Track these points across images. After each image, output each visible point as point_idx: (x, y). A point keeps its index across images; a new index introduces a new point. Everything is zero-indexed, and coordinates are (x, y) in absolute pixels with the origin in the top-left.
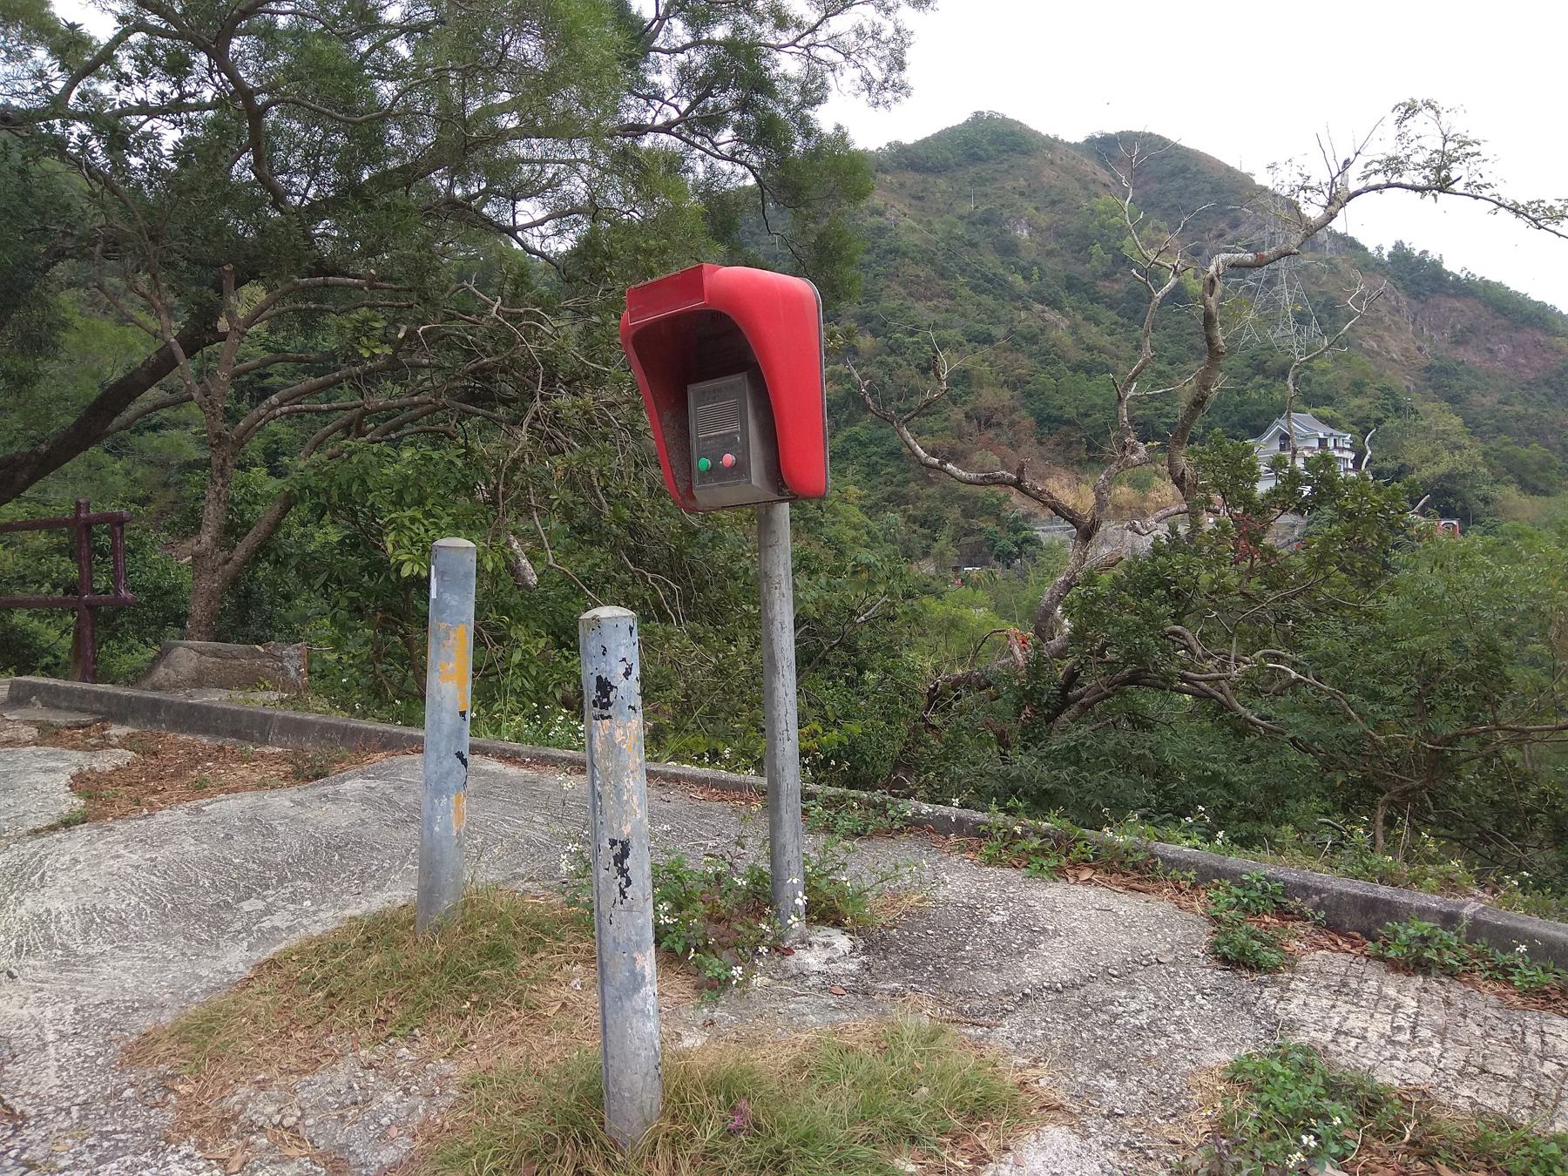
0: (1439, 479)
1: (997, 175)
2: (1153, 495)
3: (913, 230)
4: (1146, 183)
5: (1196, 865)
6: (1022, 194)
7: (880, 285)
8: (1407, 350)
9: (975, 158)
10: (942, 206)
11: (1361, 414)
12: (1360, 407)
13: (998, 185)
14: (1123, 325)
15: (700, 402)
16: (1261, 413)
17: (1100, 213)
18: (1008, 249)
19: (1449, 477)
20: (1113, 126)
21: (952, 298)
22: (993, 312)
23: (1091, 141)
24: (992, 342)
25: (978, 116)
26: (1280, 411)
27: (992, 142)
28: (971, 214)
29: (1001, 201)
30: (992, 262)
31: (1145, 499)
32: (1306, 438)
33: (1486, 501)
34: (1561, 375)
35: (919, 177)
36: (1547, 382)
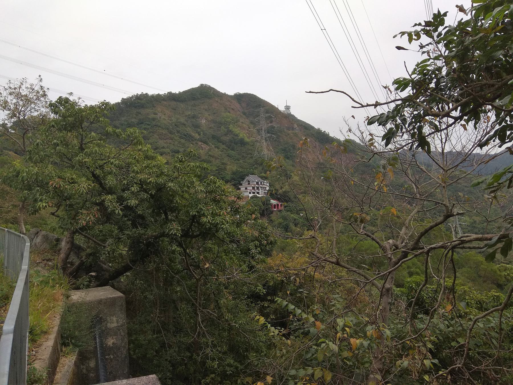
5: (488, 84)
9: (194, 99)
10: (181, 112)
13: (199, 107)
18: (197, 126)
21: (172, 139)
23: (236, 95)
25: (202, 85)
30: (190, 130)
35: (175, 103)
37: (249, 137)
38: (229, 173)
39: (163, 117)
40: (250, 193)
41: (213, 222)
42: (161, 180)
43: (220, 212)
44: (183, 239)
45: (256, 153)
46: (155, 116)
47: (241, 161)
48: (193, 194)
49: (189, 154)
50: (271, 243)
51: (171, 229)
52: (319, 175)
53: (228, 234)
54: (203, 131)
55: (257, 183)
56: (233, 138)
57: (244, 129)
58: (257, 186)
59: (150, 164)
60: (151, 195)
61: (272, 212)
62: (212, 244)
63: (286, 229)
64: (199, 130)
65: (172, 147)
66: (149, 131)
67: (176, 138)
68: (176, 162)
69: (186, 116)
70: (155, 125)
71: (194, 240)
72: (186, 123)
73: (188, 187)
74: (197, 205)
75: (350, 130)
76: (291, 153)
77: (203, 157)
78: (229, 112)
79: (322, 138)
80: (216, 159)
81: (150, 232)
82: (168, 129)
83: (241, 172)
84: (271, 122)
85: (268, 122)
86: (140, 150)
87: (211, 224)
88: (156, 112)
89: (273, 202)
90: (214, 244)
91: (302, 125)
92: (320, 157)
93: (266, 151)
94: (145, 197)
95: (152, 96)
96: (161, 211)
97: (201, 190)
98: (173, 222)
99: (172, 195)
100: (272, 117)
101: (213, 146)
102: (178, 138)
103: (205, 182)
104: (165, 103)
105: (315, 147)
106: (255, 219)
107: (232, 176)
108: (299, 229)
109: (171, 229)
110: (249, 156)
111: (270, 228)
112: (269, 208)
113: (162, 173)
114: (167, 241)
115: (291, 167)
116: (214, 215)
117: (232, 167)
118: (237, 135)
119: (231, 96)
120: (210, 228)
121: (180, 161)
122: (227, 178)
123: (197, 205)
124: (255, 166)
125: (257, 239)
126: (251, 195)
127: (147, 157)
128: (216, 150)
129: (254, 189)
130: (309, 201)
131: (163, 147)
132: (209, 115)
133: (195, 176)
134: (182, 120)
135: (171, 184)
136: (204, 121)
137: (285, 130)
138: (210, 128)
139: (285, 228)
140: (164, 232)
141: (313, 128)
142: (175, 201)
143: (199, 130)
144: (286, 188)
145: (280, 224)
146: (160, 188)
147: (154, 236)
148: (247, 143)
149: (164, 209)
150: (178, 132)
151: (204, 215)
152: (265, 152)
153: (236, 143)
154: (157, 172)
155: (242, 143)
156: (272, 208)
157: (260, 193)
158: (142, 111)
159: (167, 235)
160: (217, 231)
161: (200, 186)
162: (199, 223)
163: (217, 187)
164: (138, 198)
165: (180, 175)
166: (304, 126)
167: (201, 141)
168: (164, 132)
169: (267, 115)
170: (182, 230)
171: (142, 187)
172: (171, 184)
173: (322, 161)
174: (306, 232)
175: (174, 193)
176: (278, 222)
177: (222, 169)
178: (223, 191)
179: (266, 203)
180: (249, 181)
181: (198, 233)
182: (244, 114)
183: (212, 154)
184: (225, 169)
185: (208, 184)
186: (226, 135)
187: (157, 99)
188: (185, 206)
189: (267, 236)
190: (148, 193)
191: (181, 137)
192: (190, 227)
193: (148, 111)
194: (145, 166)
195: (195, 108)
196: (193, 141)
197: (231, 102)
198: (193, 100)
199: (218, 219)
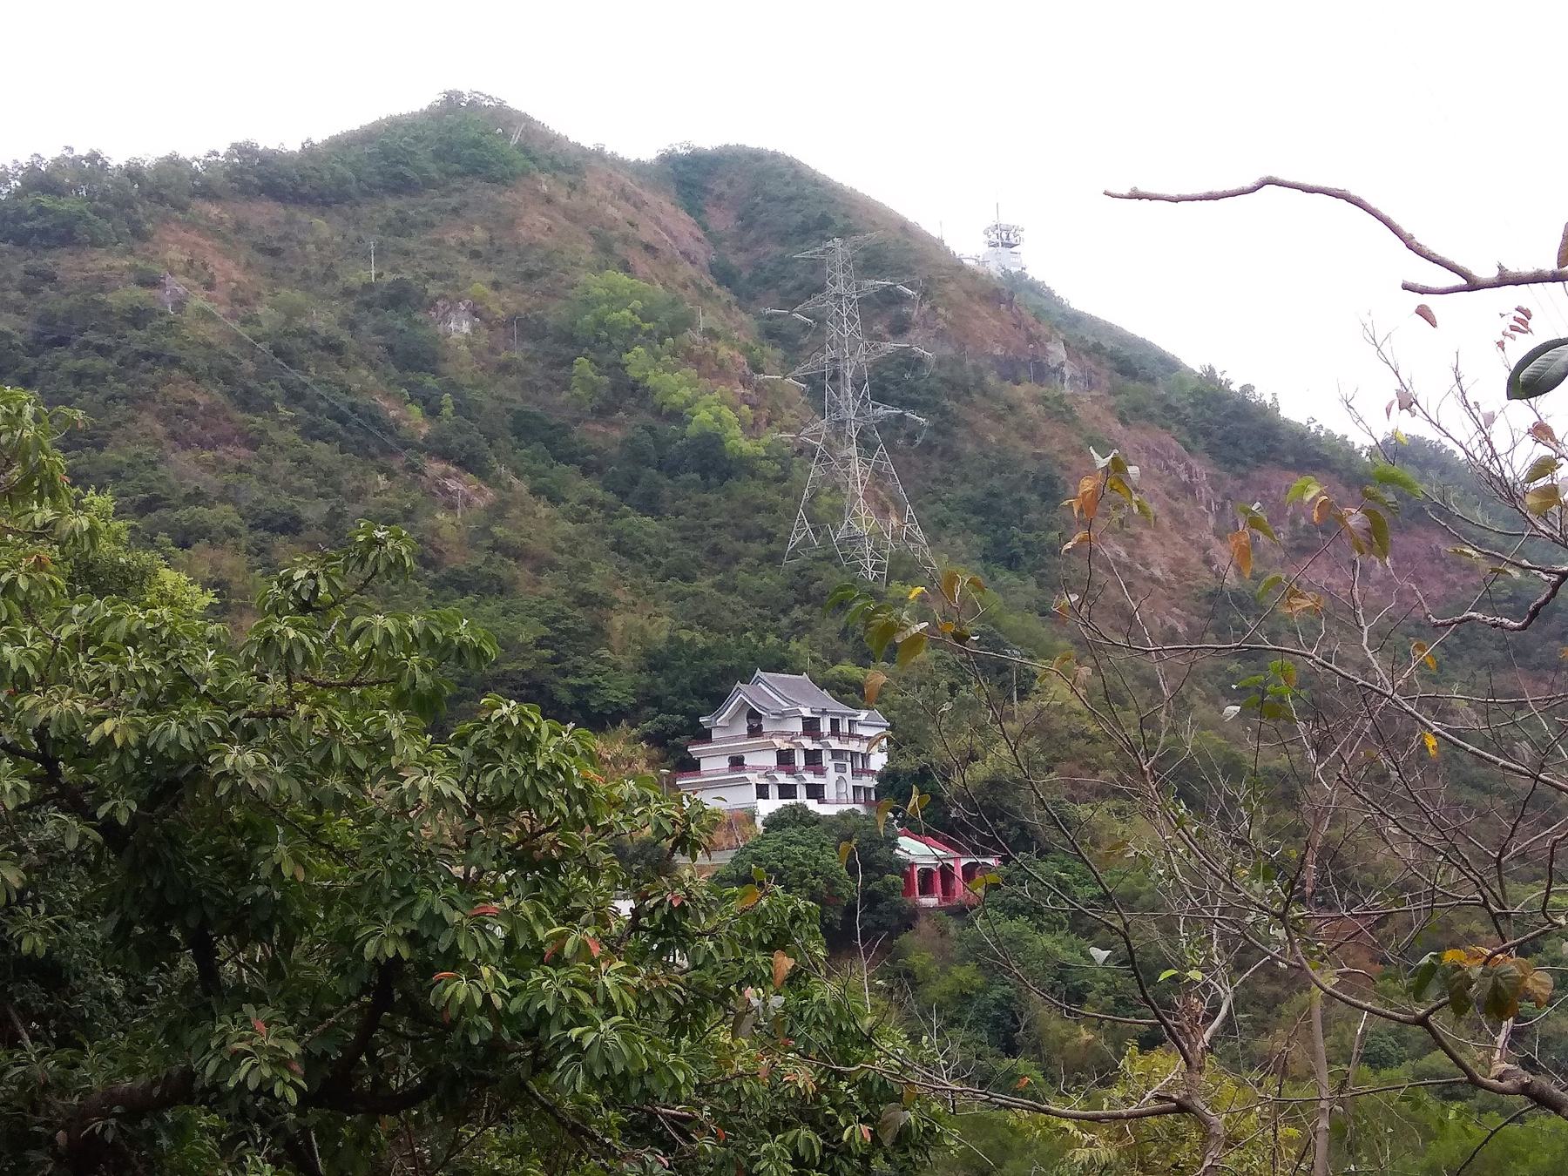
1: (435, 218)
3: (206, 316)
4: (758, 241)
6: (475, 255)
7: (115, 418)
8: (1181, 562)
9: (401, 185)
13: (434, 235)
14: (602, 506)
17: (598, 301)
18: (414, 360)
20: (708, 139)
21: (253, 445)
22: (329, 473)
23: (670, 162)
24: (296, 532)
25: (452, 100)
27: (438, 156)
28: (368, 287)
29: (430, 266)
30: (369, 386)
35: (279, 211)
37: (751, 429)
38: (626, 661)
39: (198, 300)
40: (762, 792)
41: (516, 1005)
42: (173, 730)
43: (563, 937)
44: (314, 1115)
45: (799, 532)
46: (143, 293)
47: (704, 584)
48: (387, 819)
49: (363, 560)
50: (903, 1137)
51: (239, 1056)
52: (1218, 670)
53: (616, 1086)
54: (453, 387)
55: (811, 727)
56: (651, 429)
57: (720, 372)
58: (808, 744)
59: (105, 623)
60: (109, 827)
61: (909, 919)
62: (509, 1151)
63: (1007, 1031)
64: (430, 382)
65: (255, 491)
66: (104, 392)
67: (277, 436)
68: (277, 609)
69: (348, 293)
70: (147, 356)
71: (388, 1122)
72: (345, 338)
73: (355, 777)
74: (407, 892)
75: (1407, 402)
76: (1029, 528)
77: (460, 560)
78: (626, 268)
79: (1237, 437)
80: (538, 570)
81: (94, 1072)
82: (226, 377)
83: (706, 652)
84: (900, 328)
85: (878, 327)
86: (44, 532)
87: (499, 1017)
88: (156, 268)
89: (915, 850)
90: (523, 1151)
91: (1097, 348)
92: (1222, 554)
93: (868, 518)
94: (72, 842)
95: (133, 173)
96: (176, 935)
97: (437, 796)
98: (249, 1009)
99: (248, 824)
100: (901, 299)
101: (521, 486)
102: (290, 435)
103: (462, 741)
104: (214, 211)
105: (1189, 489)
106: (794, 980)
107: (645, 679)
108: (1086, 1036)
109: (239, 1056)
110: (757, 548)
111: (893, 1045)
112: (890, 889)
113: (184, 685)
114: (212, 1131)
115: (1033, 623)
116: (519, 956)
117: (641, 622)
118: (677, 416)
119: (639, 169)
120: (494, 1047)
121: (304, 608)
122: (614, 695)
123: (407, 892)
124: (797, 613)
125: (806, 1111)
126: (770, 806)
127: (92, 577)
128: (543, 510)
129: (782, 764)
130: (1148, 842)
131: (196, 497)
132: (496, 285)
133: (399, 702)
134: (323, 320)
135: (238, 758)
136: (460, 327)
137: (991, 379)
138: (505, 368)
139: (997, 1022)
140: (189, 1076)
141: (1170, 365)
142: (265, 871)
143: (430, 382)
144: (998, 759)
145: (964, 997)
146: (170, 782)
147: (127, 1099)
148: (742, 467)
149: (192, 922)
150: (295, 396)
151: (453, 959)
152: (863, 520)
153: (670, 468)
154: (149, 675)
155: (711, 462)
156: (908, 891)
157: (830, 793)
158: (64, 263)
159: (214, 1096)
160: (542, 1066)
161: (425, 764)
162: (422, 1015)
163: (539, 776)
164: (22, 850)
165: (298, 698)
166: (1113, 357)
167: (445, 456)
168: (202, 400)
169: (874, 284)
170: (308, 1058)
171: (53, 774)
172: (238, 758)
173: (1231, 580)
174: (1133, 1063)
175: (263, 815)
176: (946, 985)
177: (581, 636)
178: (583, 797)
179: (872, 856)
180: (753, 715)
181: (415, 1076)
182: (724, 276)
183: (516, 539)
184: (598, 632)
185: (482, 752)
186: (603, 412)
187: (164, 192)
188: (328, 898)
189: (877, 1094)
190: (87, 815)
191: (311, 432)
192: (365, 1043)
193: (102, 261)
194: (74, 638)
195: (405, 243)
196: (387, 451)
197: (639, 205)
198: (396, 191)
199: (549, 986)
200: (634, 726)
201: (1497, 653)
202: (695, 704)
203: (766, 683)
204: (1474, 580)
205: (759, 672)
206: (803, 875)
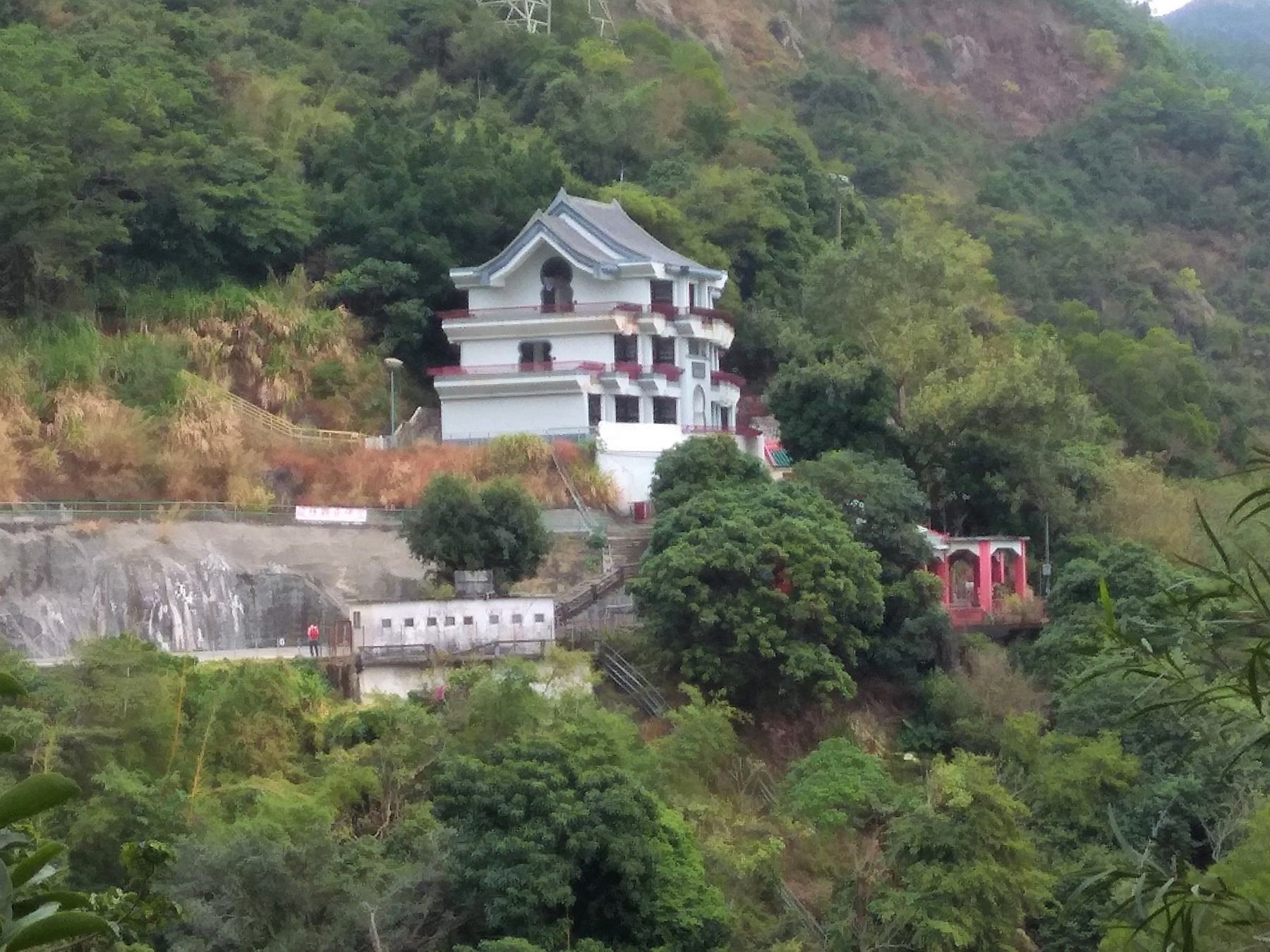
0: (970, 422)
2: (186, 427)
11: (734, 213)
12: (729, 194)
15: (513, 365)
16: (481, 191)
19: (994, 415)
26: (543, 189)
31: (160, 437)
32: (618, 276)
33: (1084, 489)
34: (1102, 133)
36: (1071, 150)
55: (661, 292)
58: (662, 327)
200: (315, 276)
201: (1143, 200)
202: (434, 246)
203: (576, 216)
204: (1101, 84)
205: (562, 195)
206: (819, 572)
